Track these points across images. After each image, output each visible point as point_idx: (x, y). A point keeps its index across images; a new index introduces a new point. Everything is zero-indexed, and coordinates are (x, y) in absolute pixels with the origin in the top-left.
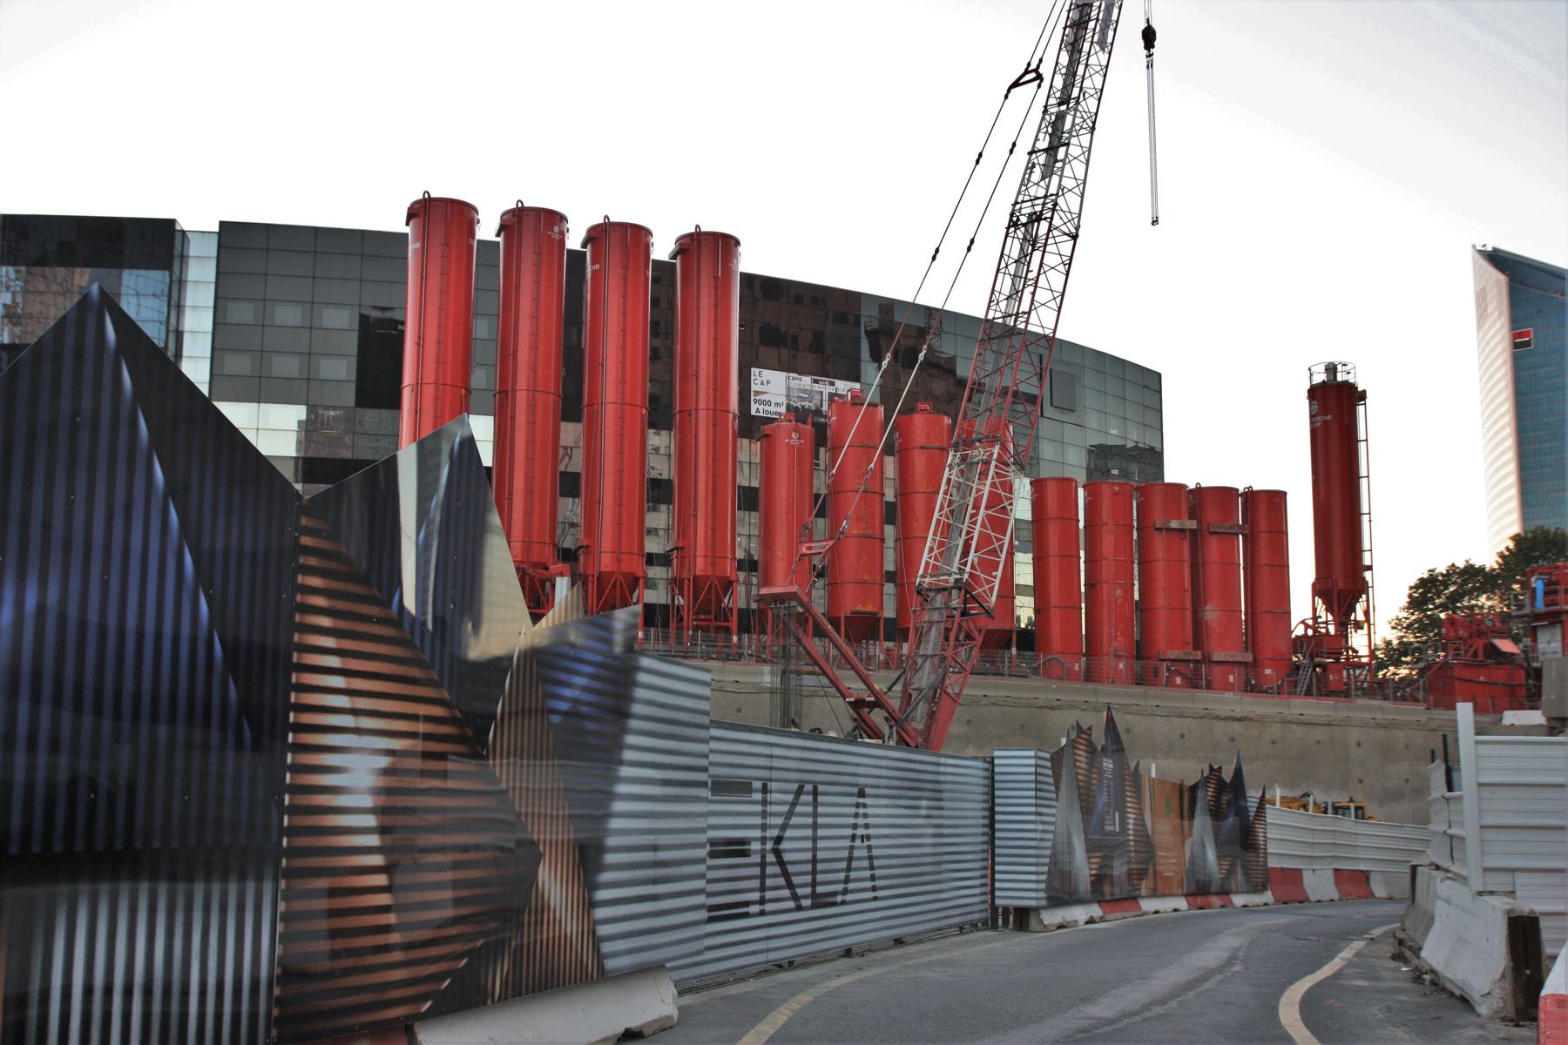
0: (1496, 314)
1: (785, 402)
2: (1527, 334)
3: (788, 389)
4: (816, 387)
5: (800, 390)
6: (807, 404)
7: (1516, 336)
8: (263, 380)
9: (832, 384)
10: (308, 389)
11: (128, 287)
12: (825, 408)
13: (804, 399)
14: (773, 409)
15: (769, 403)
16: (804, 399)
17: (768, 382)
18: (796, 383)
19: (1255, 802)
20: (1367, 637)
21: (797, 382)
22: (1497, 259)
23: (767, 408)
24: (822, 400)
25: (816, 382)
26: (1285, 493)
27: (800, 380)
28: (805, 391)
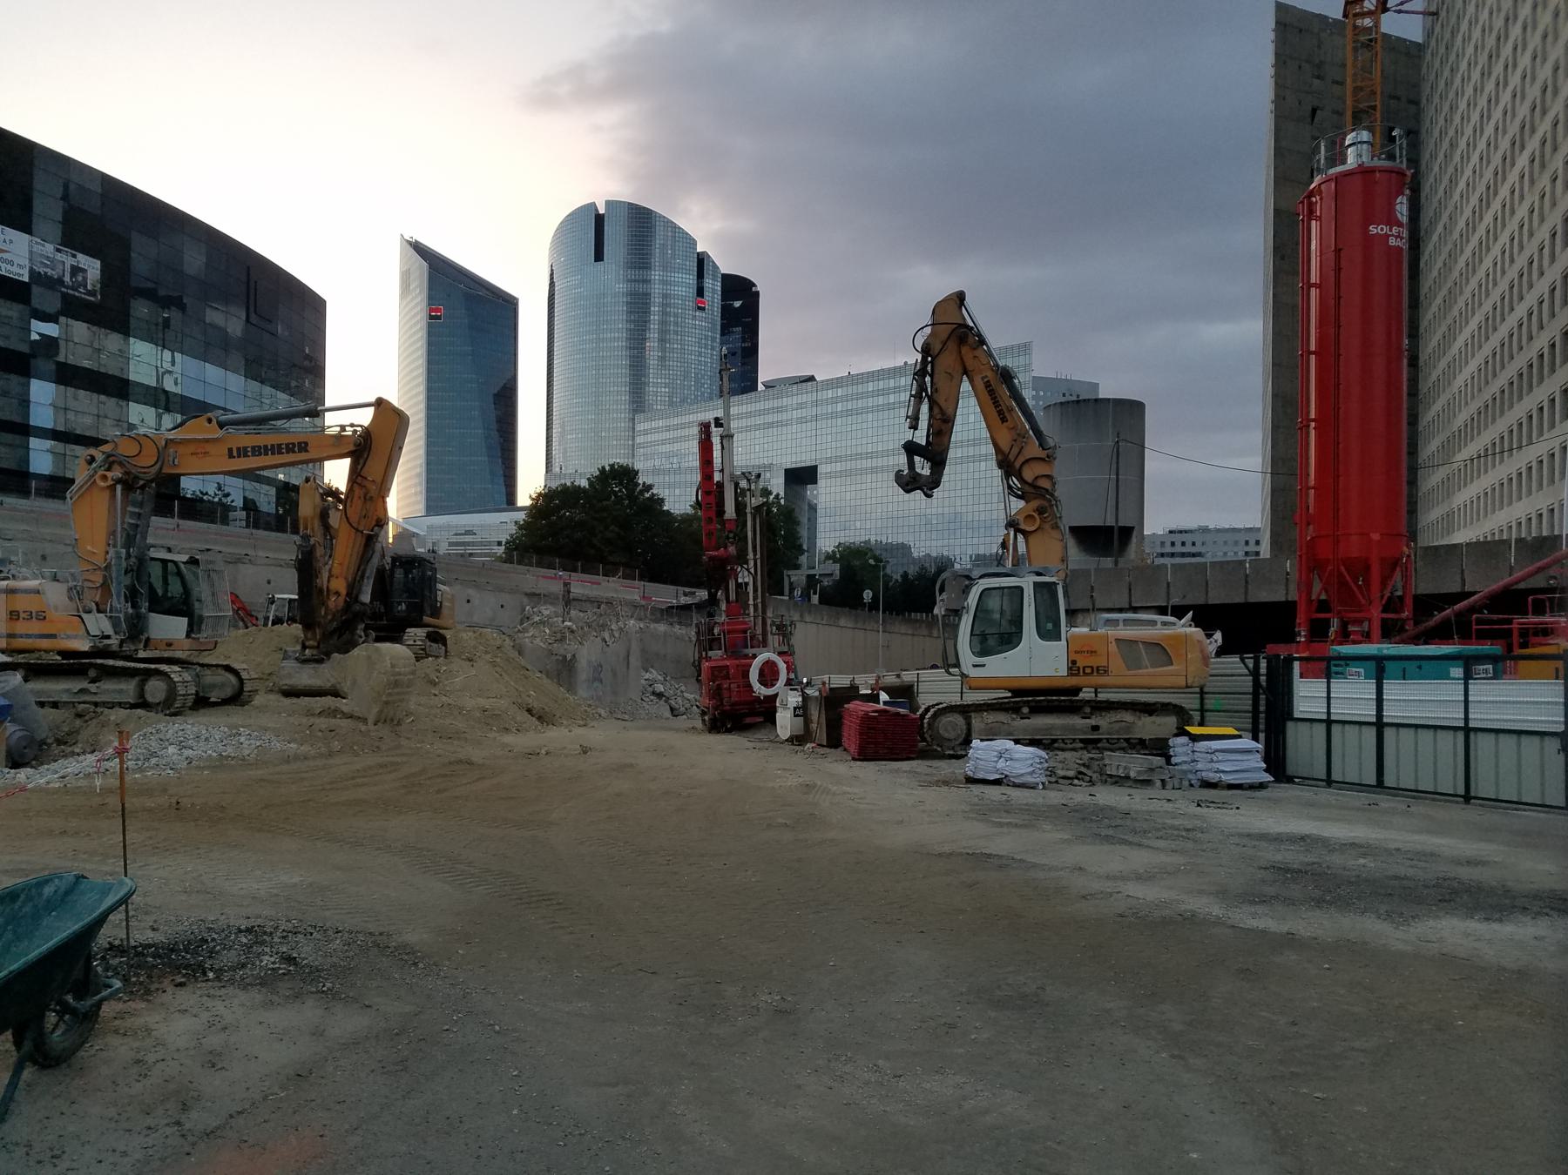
0: (418, 291)
1: (28, 265)
2: (439, 310)
3: (31, 252)
4: (59, 256)
5: (41, 255)
6: (50, 272)
7: (431, 310)
8: (1335, 729)
9: (74, 256)
10: (1416, 750)
11: (1063, 560)
12: (67, 279)
13: (46, 266)
14: (15, 269)
15: (11, 263)
16: (46, 266)
17: (11, 241)
18: (38, 248)
19: (1248, 723)
20: (1347, 726)
21: (40, 247)
22: (419, 249)
23: (9, 267)
24: (64, 270)
25: (58, 250)
26: (624, 475)
27: (43, 246)
28: (48, 258)
